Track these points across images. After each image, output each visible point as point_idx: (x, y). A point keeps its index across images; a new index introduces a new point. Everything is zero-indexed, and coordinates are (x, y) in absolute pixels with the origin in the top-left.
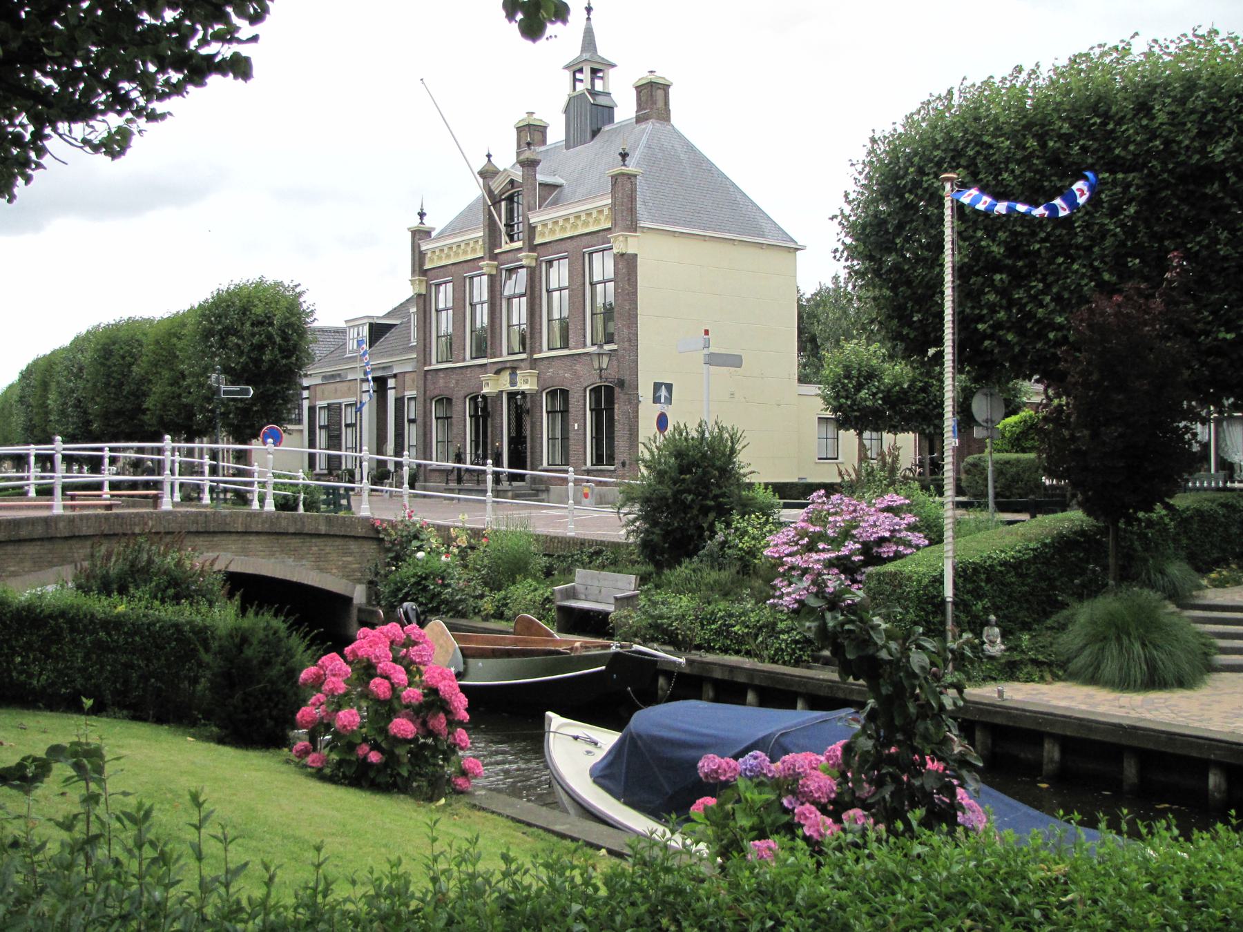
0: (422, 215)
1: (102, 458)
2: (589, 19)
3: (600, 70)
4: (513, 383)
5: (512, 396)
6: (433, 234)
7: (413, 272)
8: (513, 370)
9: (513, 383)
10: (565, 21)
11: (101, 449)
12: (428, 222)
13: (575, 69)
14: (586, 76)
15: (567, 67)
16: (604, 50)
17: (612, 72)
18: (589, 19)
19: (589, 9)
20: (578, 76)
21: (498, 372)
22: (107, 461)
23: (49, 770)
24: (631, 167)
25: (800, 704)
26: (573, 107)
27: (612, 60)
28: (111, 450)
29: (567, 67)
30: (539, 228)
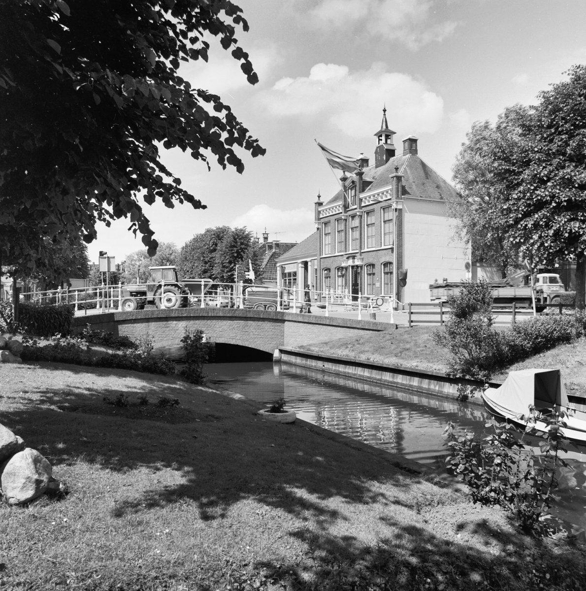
0: (319, 197)
1: (201, 285)
2: (385, 115)
3: (390, 135)
4: (354, 262)
5: (353, 267)
6: (324, 204)
7: (316, 219)
8: (354, 257)
9: (354, 262)
10: (263, 155)
11: (201, 282)
12: (322, 200)
13: (379, 135)
14: (383, 138)
15: (375, 135)
16: (391, 128)
17: (394, 135)
18: (385, 115)
19: (385, 111)
20: (380, 138)
21: (348, 258)
22: (203, 287)
23: (245, 73)
24: (400, 174)
25: (209, 148)
26: (379, 151)
27: (394, 131)
28: (205, 282)
29: (375, 135)
30: (364, 200)
